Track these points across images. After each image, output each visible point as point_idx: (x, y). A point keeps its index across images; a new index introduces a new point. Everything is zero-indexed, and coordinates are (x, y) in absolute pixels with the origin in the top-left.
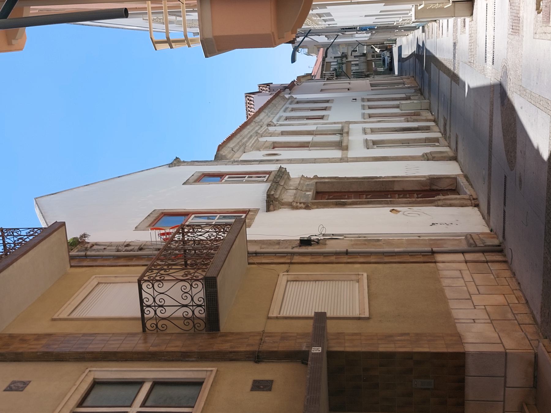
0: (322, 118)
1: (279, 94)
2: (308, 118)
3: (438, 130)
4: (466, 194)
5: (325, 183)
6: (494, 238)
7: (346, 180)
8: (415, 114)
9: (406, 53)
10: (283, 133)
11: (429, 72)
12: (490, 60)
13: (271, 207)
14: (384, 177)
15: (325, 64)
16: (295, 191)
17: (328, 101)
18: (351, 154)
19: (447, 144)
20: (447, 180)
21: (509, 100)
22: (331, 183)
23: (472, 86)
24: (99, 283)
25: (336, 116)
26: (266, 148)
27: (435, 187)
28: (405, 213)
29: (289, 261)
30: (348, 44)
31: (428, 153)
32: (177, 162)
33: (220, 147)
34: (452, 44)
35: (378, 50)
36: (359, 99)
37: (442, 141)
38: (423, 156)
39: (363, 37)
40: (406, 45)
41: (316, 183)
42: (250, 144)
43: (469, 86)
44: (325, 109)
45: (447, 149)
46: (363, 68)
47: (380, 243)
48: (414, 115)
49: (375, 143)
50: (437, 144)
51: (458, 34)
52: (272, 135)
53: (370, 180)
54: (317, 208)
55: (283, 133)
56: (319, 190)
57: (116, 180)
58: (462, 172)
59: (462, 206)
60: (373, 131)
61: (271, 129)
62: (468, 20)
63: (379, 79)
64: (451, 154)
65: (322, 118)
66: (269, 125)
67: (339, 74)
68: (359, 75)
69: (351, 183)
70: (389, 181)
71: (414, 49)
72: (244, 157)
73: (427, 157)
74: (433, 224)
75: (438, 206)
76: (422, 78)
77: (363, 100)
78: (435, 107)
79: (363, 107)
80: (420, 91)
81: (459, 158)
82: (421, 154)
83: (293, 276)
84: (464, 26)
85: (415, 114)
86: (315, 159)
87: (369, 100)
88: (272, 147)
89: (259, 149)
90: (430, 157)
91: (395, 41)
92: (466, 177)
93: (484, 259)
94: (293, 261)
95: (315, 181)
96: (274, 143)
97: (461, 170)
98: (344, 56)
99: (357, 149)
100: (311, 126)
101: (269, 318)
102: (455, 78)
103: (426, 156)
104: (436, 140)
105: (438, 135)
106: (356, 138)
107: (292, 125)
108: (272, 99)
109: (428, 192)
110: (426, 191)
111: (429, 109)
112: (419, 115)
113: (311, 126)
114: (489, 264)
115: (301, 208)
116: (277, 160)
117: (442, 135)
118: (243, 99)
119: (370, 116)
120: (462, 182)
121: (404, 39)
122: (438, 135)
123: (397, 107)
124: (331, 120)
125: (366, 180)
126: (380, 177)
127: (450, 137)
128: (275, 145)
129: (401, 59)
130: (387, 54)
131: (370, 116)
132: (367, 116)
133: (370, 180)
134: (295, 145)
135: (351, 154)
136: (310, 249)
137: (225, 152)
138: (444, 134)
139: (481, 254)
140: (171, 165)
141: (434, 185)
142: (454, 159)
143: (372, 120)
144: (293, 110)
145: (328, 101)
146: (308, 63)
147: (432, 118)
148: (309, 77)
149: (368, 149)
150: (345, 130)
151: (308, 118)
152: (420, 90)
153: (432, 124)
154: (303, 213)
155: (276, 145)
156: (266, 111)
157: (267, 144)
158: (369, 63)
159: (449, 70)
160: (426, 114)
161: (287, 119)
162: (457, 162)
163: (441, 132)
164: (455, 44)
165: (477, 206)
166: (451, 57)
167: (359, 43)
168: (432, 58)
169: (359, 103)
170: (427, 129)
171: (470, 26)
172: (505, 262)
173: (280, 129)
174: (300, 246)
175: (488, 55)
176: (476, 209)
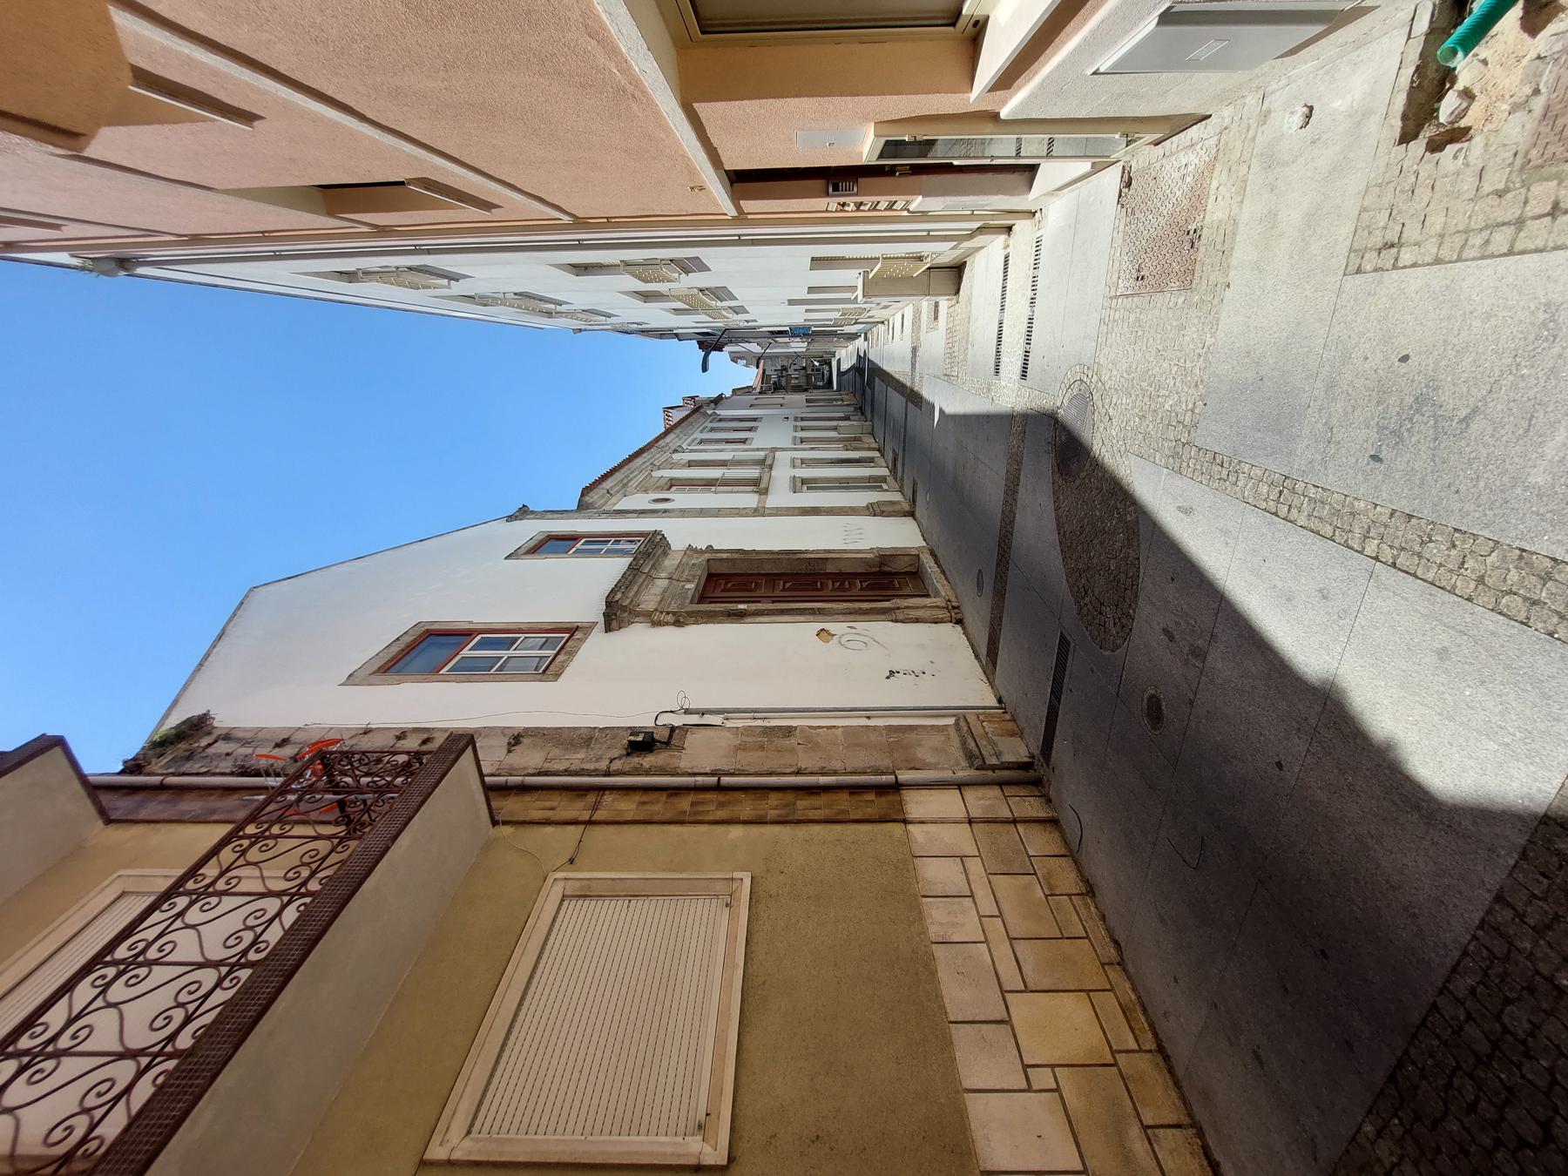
0: (744, 441)
1: (698, 409)
2: (728, 441)
4: (937, 594)
5: (721, 560)
6: (1013, 734)
7: (754, 556)
8: (855, 439)
9: (845, 366)
10: (691, 464)
11: (873, 389)
12: (1011, 365)
13: (614, 624)
15: (765, 377)
17: (755, 420)
18: (772, 501)
21: (1097, 466)
22: (727, 559)
23: (949, 410)
24: (123, 894)
25: (762, 439)
26: (660, 489)
27: (886, 569)
28: (843, 640)
29: (586, 816)
30: (787, 356)
32: (524, 512)
33: (586, 491)
34: (909, 350)
38: (867, 508)
39: (798, 346)
40: (846, 357)
42: (633, 484)
43: (941, 411)
44: (750, 429)
45: (897, 497)
46: (803, 381)
47: (793, 741)
48: (852, 442)
51: (922, 334)
52: (673, 466)
54: (696, 623)
55: (691, 464)
57: (414, 547)
61: (676, 456)
62: (944, 303)
63: (815, 394)
64: (906, 507)
65: (744, 441)
66: (676, 451)
67: (777, 388)
68: (798, 389)
71: (854, 361)
72: (624, 504)
73: (874, 510)
74: (892, 673)
76: (863, 394)
77: (796, 419)
78: (879, 432)
80: (861, 410)
81: (918, 515)
83: (578, 884)
84: (936, 318)
85: (855, 439)
87: (802, 419)
89: (646, 491)
91: (834, 354)
92: (933, 554)
93: (1006, 814)
94: (600, 815)
95: (707, 556)
98: (784, 369)
99: (780, 496)
101: (424, 1164)
102: (914, 398)
105: (885, 472)
106: (782, 473)
108: (688, 416)
109: (875, 585)
110: (874, 574)
111: (872, 434)
112: (859, 439)
114: (1021, 828)
115: (667, 624)
116: (666, 511)
118: (662, 415)
120: (928, 562)
121: (843, 351)
122: (885, 472)
123: (835, 429)
126: (806, 552)
128: (672, 483)
129: (840, 373)
130: (826, 368)
135: (772, 501)
136: (648, 760)
137: (593, 497)
138: (894, 471)
139: (995, 792)
140: (510, 518)
142: (911, 514)
143: (804, 446)
144: (712, 430)
145: (755, 420)
146: (749, 376)
147: (875, 445)
148: (747, 390)
150: (768, 462)
151: (728, 441)
153: (877, 454)
154: (669, 633)
156: (677, 431)
157: (661, 482)
158: (808, 377)
159: (904, 386)
160: (869, 440)
164: (914, 350)
165: (959, 622)
166: (908, 368)
167: (798, 355)
168: (877, 372)
169: (791, 423)
171: (950, 315)
172: (1054, 822)
174: (628, 754)
175: (1004, 359)
176: (959, 628)
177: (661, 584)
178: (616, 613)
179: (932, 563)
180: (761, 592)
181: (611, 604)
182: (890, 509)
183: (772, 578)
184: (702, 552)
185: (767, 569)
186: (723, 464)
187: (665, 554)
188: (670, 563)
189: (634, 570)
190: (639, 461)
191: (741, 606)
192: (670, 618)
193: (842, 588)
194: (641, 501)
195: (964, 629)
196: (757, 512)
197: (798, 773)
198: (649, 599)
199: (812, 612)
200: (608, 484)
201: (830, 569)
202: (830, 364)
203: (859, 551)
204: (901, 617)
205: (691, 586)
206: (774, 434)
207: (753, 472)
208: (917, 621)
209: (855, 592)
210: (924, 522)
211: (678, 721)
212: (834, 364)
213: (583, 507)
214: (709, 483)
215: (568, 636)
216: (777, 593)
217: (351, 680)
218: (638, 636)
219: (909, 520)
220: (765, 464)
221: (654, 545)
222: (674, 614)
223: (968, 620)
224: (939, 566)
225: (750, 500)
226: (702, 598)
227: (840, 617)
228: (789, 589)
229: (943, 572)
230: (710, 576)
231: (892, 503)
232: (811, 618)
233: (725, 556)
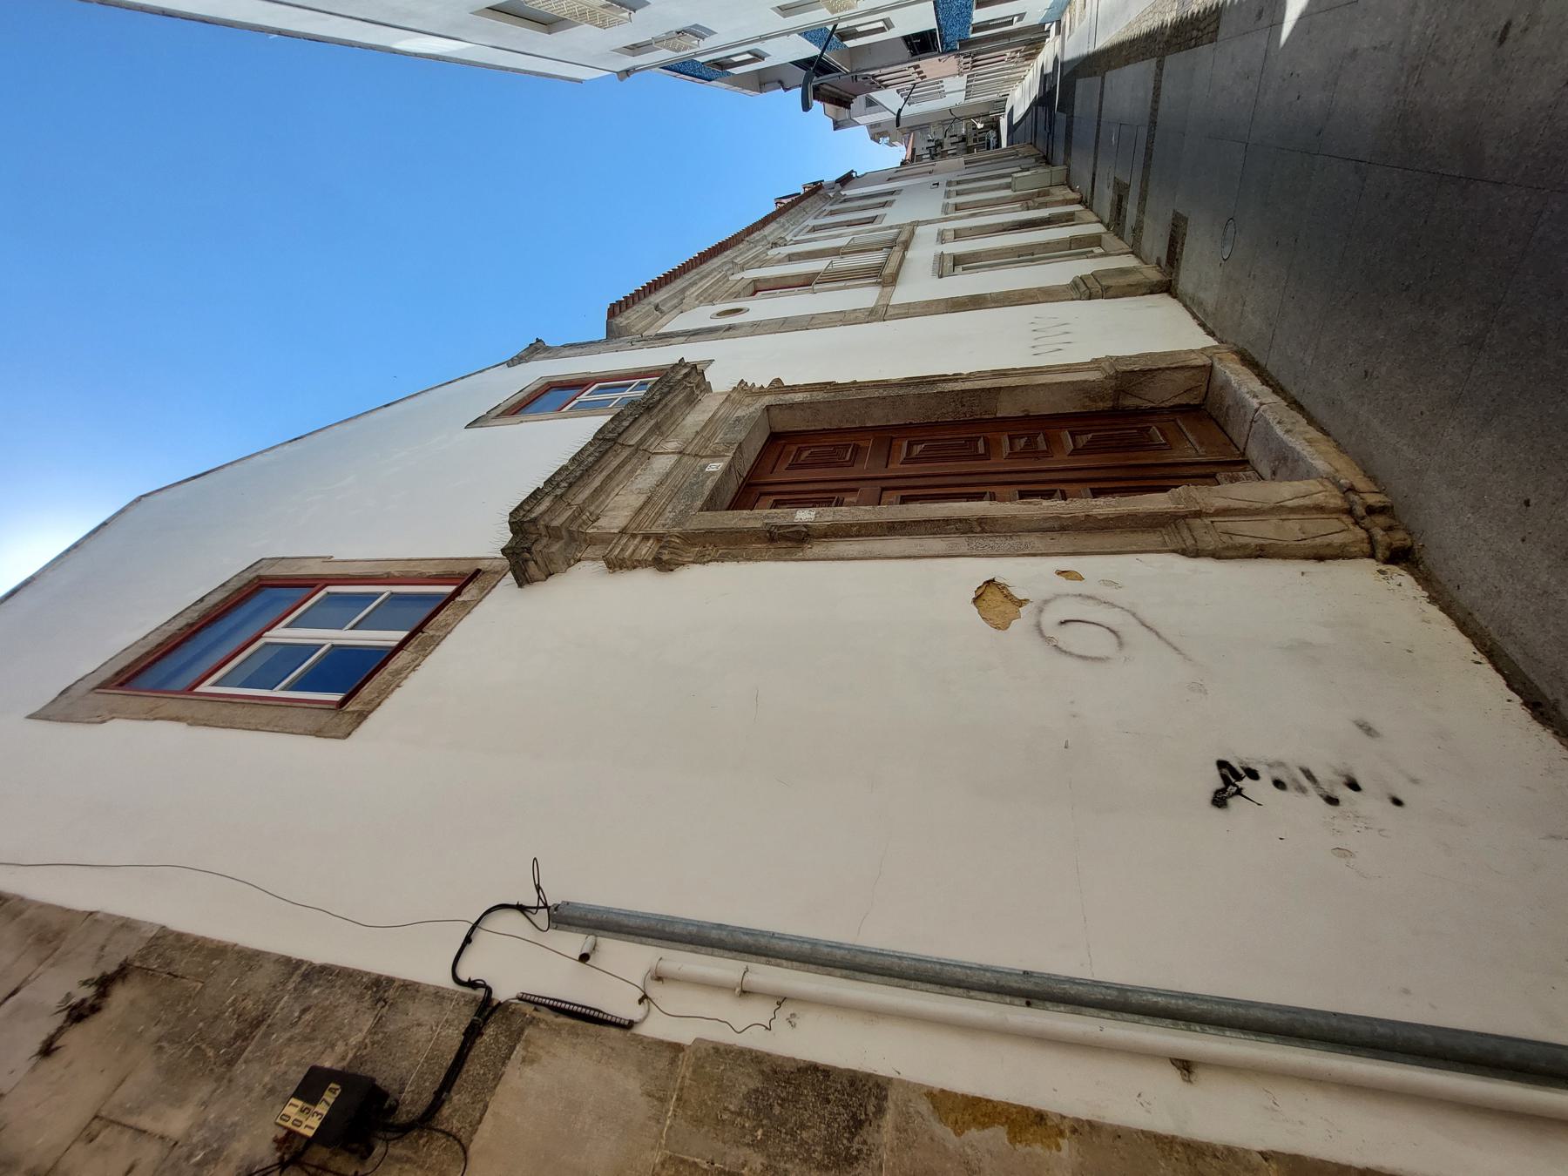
0: (872, 220)
3: (1095, 219)
4: (1286, 464)
5: (791, 406)
7: (854, 395)
8: (1039, 195)
14: (970, 377)
16: (676, 457)
17: (892, 193)
19: (1127, 248)
20: (1179, 376)
22: (810, 405)
27: (1130, 402)
28: (1050, 617)
31: (1087, 277)
32: (537, 349)
33: (615, 310)
35: (980, 126)
36: (943, 183)
37: (1110, 240)
38: (1074, 285)
41: (768, 408)
44: (884, 205)
45: (1129, 262)
49: (959, 261)
50: (1097, 250)
53: (924, 390)
54: (701, 560)
55: (791, 258)
56: (779, 428)
58: (1211, 333)
59: (1320, 558)
60: (958, 235)
63: (976, 155)
64: (1153, 275)
65: (872, 220)
66: (775, 245)
69: (868, 402)
70: (983, 390)
73: (1086, 289)
75: (1195, 553)
77: (949, 184)
79: (948, 195)
82: (1068, 281)
85: (1039, 195)
86: (813, 317)
87: (958, 183)
88: (751, 289)
89: (712, 302)
90: (1096, 288)
95: (767, 400)
96: (755, 281)
97: (1202, 325)
99: (919, 284)
100: (863, 235)
103: (1083, 288)
104: (1096, 240)
105: (1097, 228)
106: (923, 252)
107: (815, 240)
111: (1068, 183)
112: (1047, 194)
113: (863, 235)
116: (730, 328)
117: (1108, 227)
119: (957, 208)
122: (1097, 228)
123: (1008, 186)
124: (885, 223)
125: (914, 391)
126: (956, 378)
127: (1138, 229)
130: (992, 134)
131: (957, 208)
132: (951, 208)
133: (924, 390)
134: (795, 282)
135: (903, 294)
138: (1116, 223)
140: (511, 363)
141: (1126, 392)
142: (1167, 288)
144: (832, 213)
149: (941, 277)
151: (850, 224)
152: (1045, 157)
155: (760, 286)
157: (739, 287)
160: (1062, 193)
161: (814, 229)
162: (1175, 296)
163: (1101, 222)
165: (1401, 557)
170: (1068, 219)
173: (785, 251)
176: (1403, 579)
177: (662, 464)
178: (539, 541)
179: (1256, 385)
180: (864, 467)
181: (521, 522)
182: (1123, 281)
183: (886, 436)
184: (762, 392)
185: (877, 418)
186: (836, 252)
187: (691, 401)
188: (695, 419)
189: (606, 441)
190: (716, 262)
191: (804, 515)
192: (647, 550)
193: (1031, 451)
194: (701, 316)
195: (1425, 580)
196: (875, 315)
197: (1185, 1066)
198: (618, 509)
199: (965, 527)
200: (656, 298)
201: (1007, 409)
202: (997, 128)
203: (1068, 369)
204: (1209, 541)
205: (716, 466)
206: (920, 207)
207: (875, 258)
208: (1261, 552)
209: (1061, 459)
210: (1209, 298)
211: (519, 966)
212: (1004, 122)
213: (614, 334)
214: (807, 282)
215: (433, 600)
216: (897, 468)
217: (31, 717)
218: (584, 595)
219: (1164, 303)
220: (901, 242)
221: (683, 383)
222: (659, 538)
223: (1446, 527)
224: (1278, 389)
225: (865, 296)
226: (747, 493)
227: (1036, 542)
228: (917, 460)
229: (1295, 404)
230: (775, 438)
231: (1123, 272)
232: (961, 543)
233: (798, 397)
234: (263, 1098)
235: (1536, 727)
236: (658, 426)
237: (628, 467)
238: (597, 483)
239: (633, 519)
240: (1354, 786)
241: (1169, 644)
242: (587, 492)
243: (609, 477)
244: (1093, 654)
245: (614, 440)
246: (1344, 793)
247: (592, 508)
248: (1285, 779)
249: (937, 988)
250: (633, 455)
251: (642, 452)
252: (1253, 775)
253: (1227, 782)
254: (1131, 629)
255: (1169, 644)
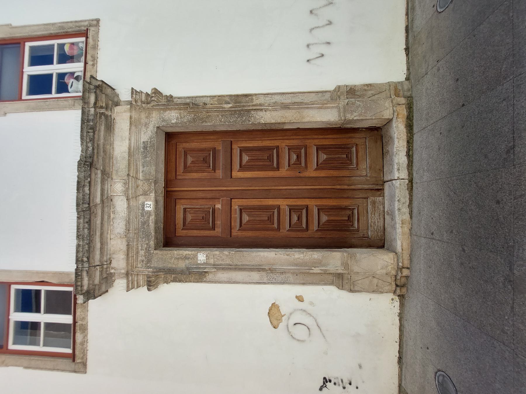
165: (402, 297)
234: (114, 253)
235: (397, 364)
236: (104, 173)
237: (106, 217)
238: (98, 245)
239: (127, 263)
240: (350, 384)
241: (323, 334)
242: (98, 252)
243: (102, 234)
244: (301, 339)
245: (89, 208)
246: (347, 386)
247: (105, 258)
248: (337, 383)
249: (274, 127)
250: (103, 208)
251: (107, 200)
252: (330, 381)
253: (324, 383)
254: (314, 328)
255: (323, 334)
